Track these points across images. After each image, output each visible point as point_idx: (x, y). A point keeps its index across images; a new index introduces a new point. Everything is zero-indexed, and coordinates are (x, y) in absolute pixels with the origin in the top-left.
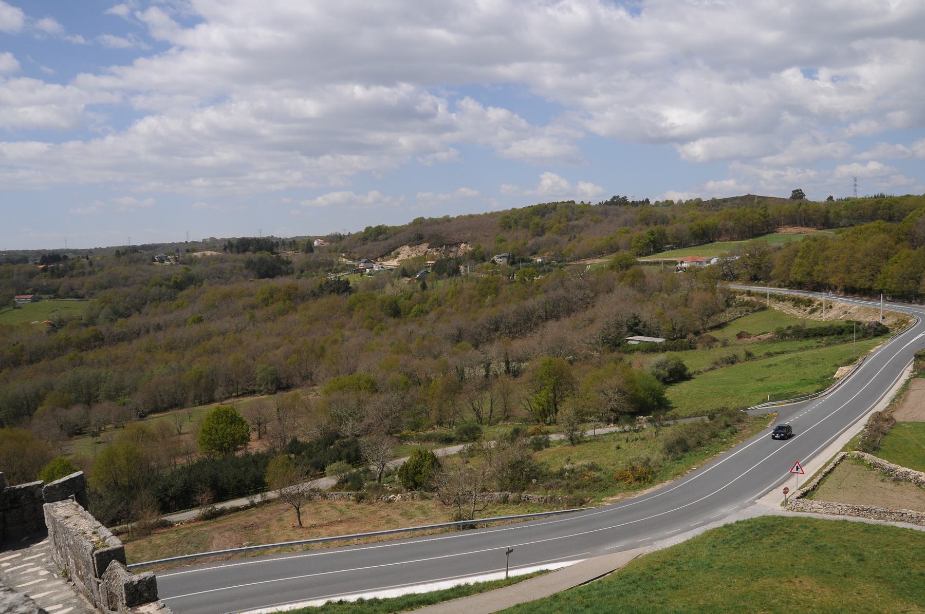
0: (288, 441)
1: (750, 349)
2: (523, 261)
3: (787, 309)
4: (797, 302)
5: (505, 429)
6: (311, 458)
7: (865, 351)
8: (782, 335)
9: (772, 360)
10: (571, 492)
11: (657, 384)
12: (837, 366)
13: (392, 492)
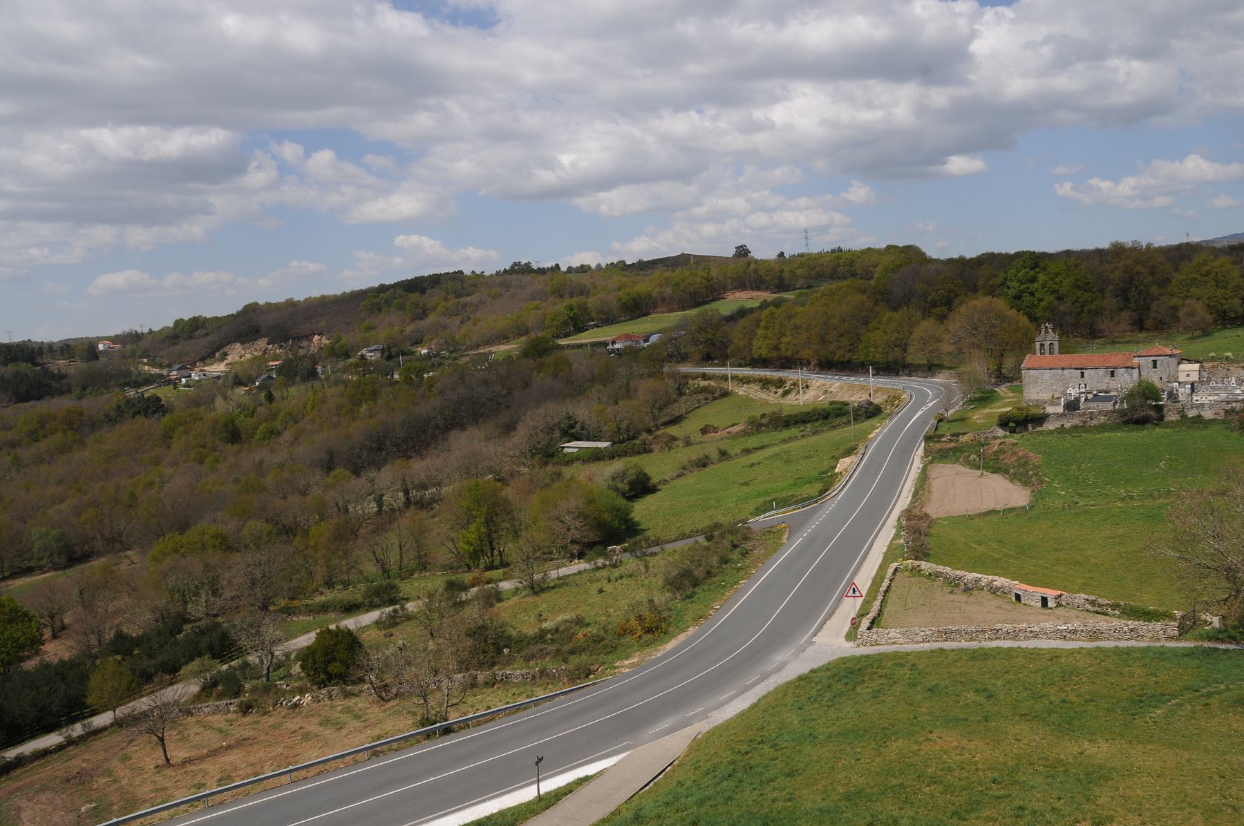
0: (109, 636)
1: (724, 445)
2: (404, 354)
3: (753, 392)
4: (765, 383)
5: (435, 582)
6: (149, 659)
7: (863, 437)
8: (756, 426)
9: (753, 458)
10: (565, 661)
11: (621, 502)
12: (837, 459)
13: (293, 692)
